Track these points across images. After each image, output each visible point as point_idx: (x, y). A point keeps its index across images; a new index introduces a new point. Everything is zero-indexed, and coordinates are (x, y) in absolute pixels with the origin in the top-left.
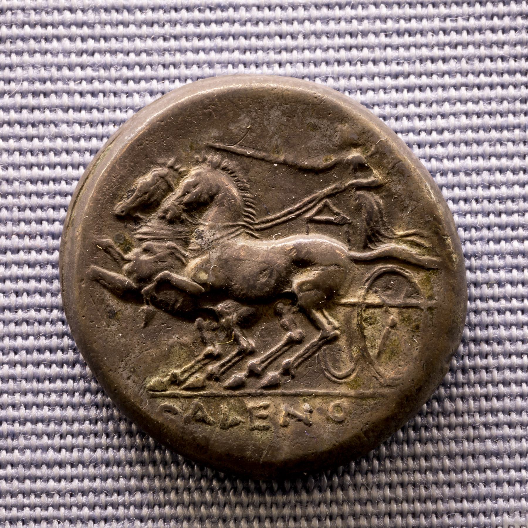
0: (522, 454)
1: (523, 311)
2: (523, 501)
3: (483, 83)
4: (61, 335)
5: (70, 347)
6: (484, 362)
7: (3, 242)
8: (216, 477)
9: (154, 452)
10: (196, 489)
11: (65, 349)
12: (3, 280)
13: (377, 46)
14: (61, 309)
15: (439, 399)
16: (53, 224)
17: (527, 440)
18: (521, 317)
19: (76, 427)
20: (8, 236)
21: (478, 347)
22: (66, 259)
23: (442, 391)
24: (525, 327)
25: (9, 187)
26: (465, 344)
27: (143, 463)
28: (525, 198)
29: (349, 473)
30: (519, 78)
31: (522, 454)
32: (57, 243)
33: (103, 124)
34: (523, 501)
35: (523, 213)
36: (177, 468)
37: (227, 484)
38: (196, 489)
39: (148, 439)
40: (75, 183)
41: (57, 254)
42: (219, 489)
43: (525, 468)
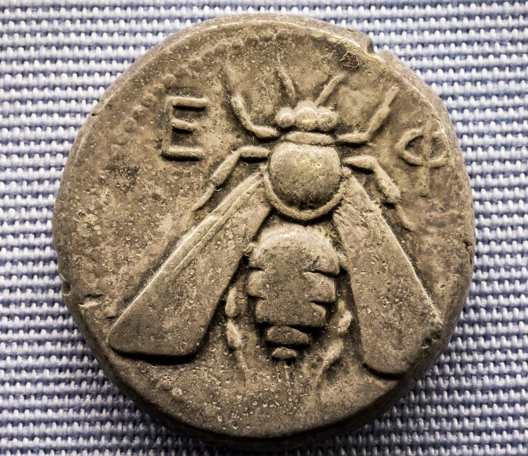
0: (523, 67)
1: (524, 226)
2: (523, 297)
3: (481, 65)
4: (73, 342)
6: (485, 275)
10: (194, 448)
11: (84, 394)
12: (2, 196)
15: (441, 366)
17: (526, 391)
18: (521, 232)
23: (443, 357)
24: (525, 122)
25: (54, 414)
26: (465, 311)
28: (525, 15)
30: (518, 192)
31: (523, 67)
32: (60, 174)
34: (523, 297)
35: (521, 28)
41: (58, 184)
43: (525, 80)
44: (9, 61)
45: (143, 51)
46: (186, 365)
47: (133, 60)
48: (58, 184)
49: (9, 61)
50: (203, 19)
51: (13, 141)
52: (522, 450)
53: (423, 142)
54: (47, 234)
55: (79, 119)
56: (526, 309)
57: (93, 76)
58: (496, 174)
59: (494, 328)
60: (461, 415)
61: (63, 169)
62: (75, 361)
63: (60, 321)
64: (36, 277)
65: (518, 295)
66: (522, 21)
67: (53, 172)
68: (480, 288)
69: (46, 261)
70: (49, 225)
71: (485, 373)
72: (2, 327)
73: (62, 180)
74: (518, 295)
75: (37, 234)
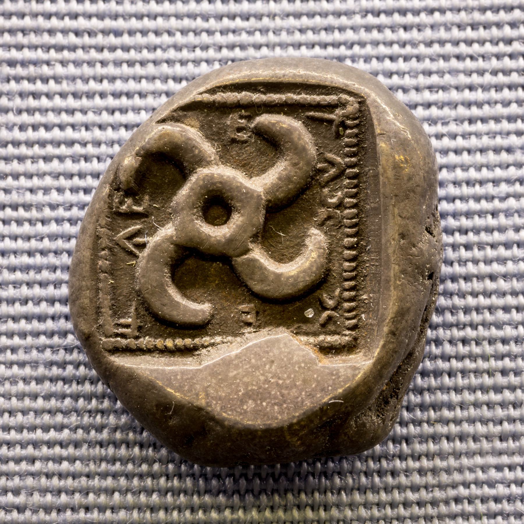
2: (519, 392)
34: (519, 392)
45: (164, 99)
47: (154, 109)
48: (73, 242)
50: (233, 61)
51: (10, 206)
53: (328, 411)
54: (64, 301)
55: (90, 181)
57: (135, 36)
59: (513, 395)
60: (460, 495)
63: (88, 387)
64: (25, 431)
67: (67, 227)
68: (392, 496)
70: (64, 291)
71: (434, 514)
75: (52, 301)
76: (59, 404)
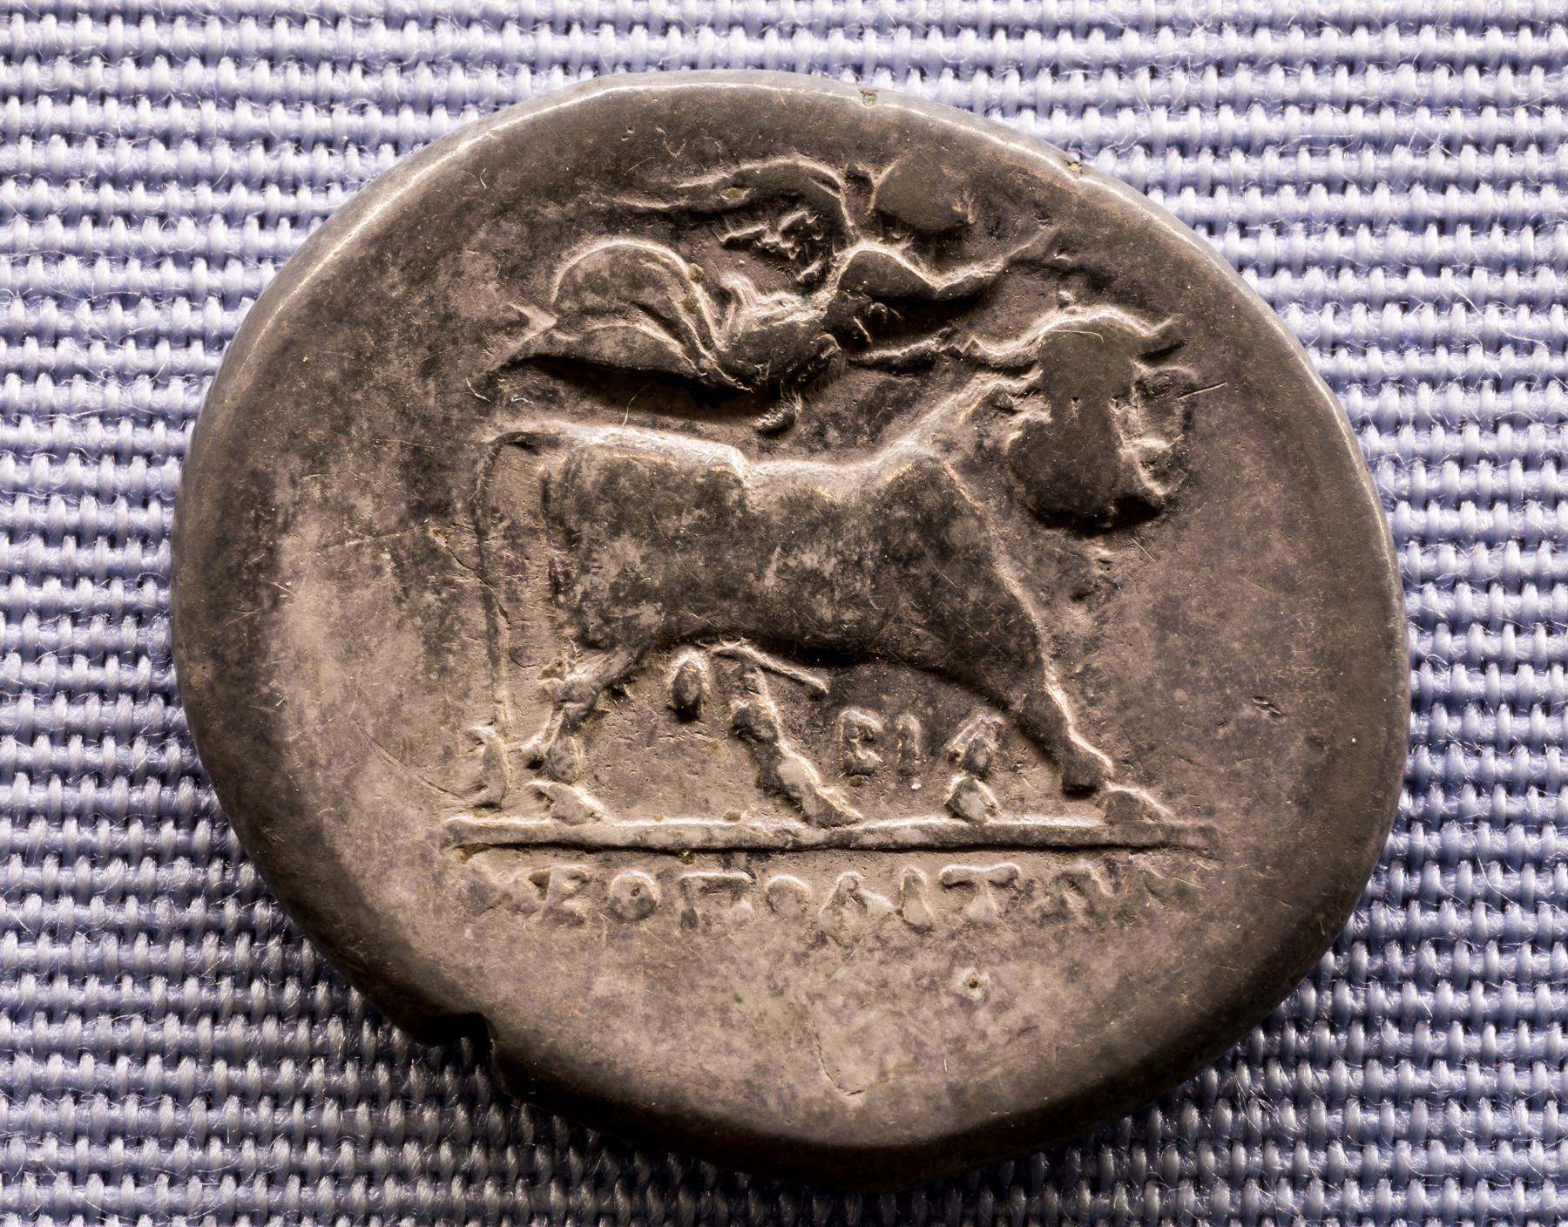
0: (1548, 64)
5: (184, 772)
7: (8, 470)
8: (545, 1138)
9: (373, 1068)
10: (585, 1176)
13: (31, 334)
14: (165, 658)
16: (1417, 33)
19: (191, 990)
20: (21, 453)
21: (1421, 801)
22: (189, 525)
27: (343, 1099)
29: (1114, 1144)
30: (1545, 1078)
33: (330, 143)
34: (1550, 831)
36: (505, 1117)
37: (606, 1162)
38: (585, 1176)
39: (389, 1033)
40: (248, 304)
42: (649, 1181)
44: (27, 176)
46: (559, 1074)
49: (27, 176)
52: (1552, 1198)
56: (1563, 504)
58: (1470, 462)
61: (191, 426)
62: (226, 991)
65: (1537, 745)
66: (1551, 478)
69: (146, 538)
72: (7, 886)
73: (187, 457)
74: (1537, 745)
76: (145, 1115)
